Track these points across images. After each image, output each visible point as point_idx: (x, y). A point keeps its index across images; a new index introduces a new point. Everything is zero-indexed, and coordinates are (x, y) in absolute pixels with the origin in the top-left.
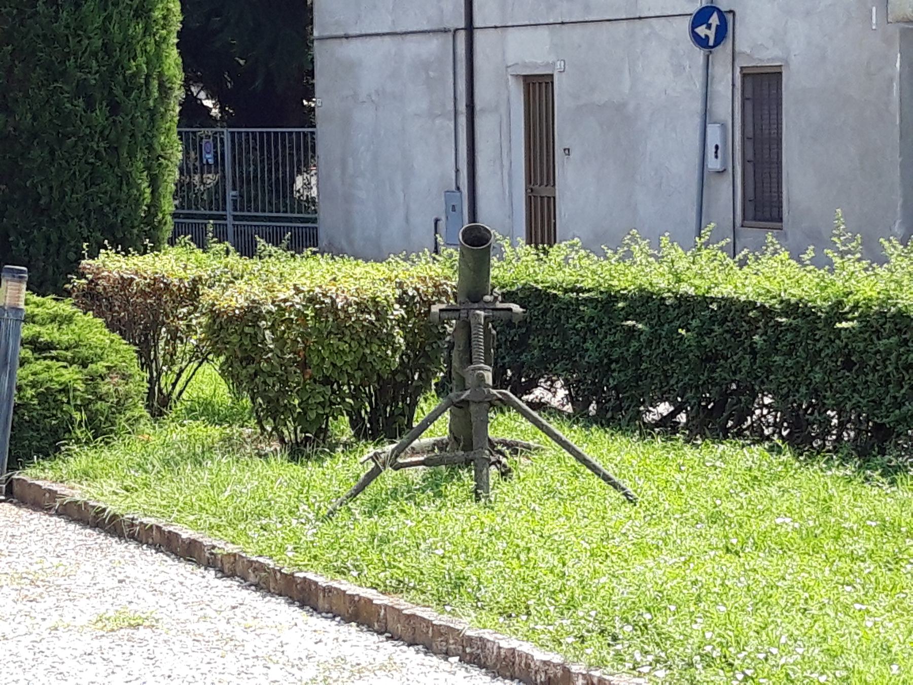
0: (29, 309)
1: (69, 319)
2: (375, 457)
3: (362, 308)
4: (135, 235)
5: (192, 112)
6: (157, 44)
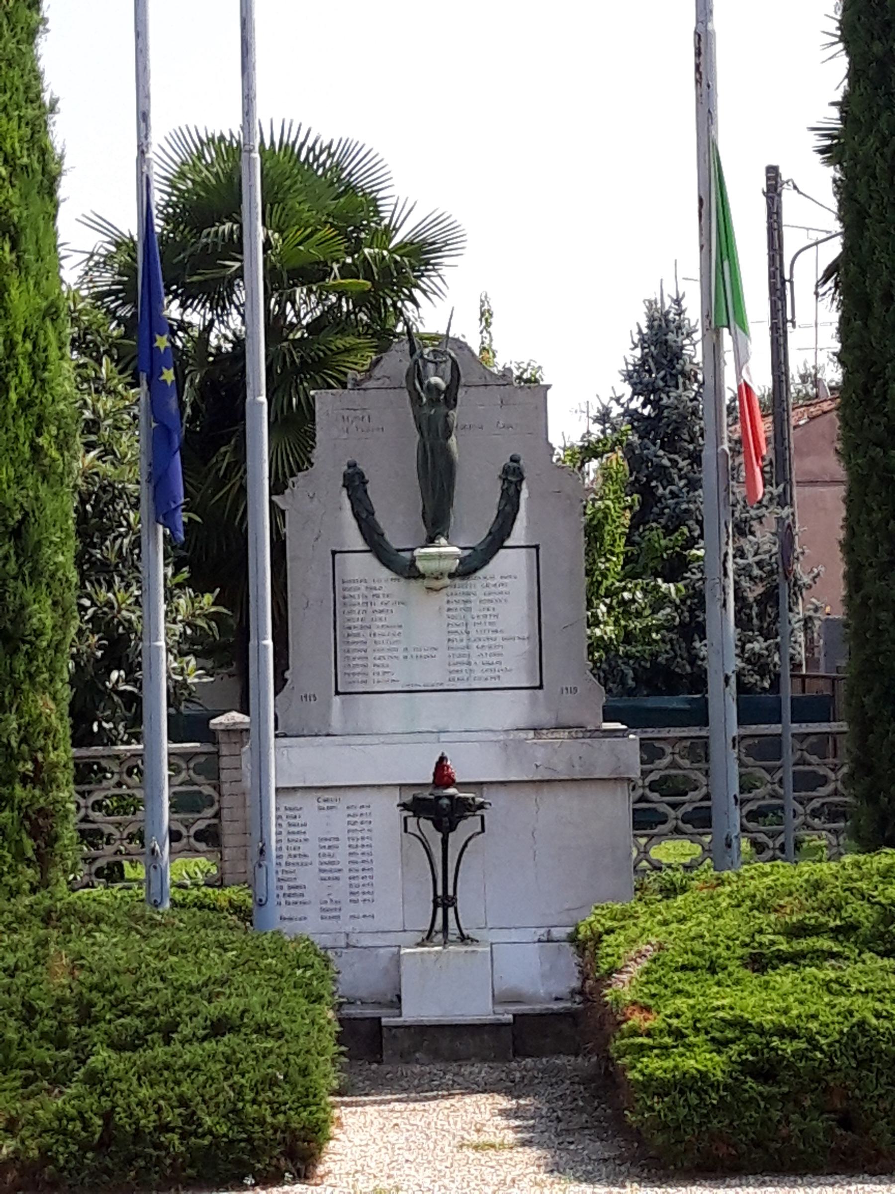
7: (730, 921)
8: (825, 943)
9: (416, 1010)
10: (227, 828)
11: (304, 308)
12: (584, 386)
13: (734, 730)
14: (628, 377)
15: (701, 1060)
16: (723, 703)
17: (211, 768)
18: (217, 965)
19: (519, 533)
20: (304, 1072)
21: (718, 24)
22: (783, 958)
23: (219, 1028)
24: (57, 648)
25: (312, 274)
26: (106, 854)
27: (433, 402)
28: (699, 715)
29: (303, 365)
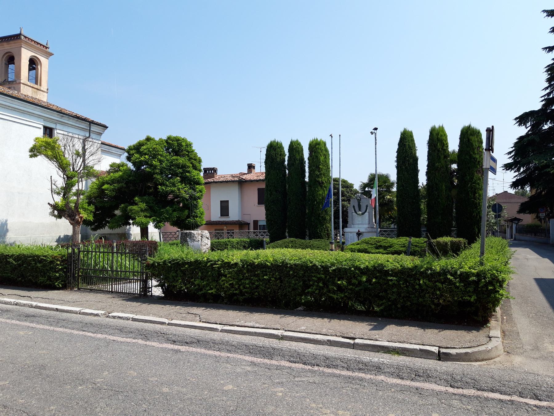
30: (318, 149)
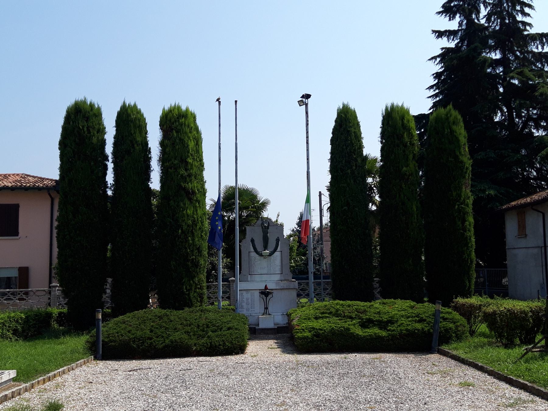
0: (442, 310)
1: (451, 313)
2: (526, 349)
3: (521, 313)
4: (466, 294)
5: (478, 265)
6: (470, 252)
7: (312, 311)
8: (327, 315)
9: (261, 326)
10: (231, 296)
11: (245, 214)
12: (289, 226)
13: (313, 281)
14: (297, 224)
15: (307, 334)
16: (311, 276)
17: (229, 287)
18: (229, 318)
19: (279, 249)
20: (243, 336)
21: (310, 170)
22: (320, 317)
23: (229, 329)
24: (204, 267)
25: (246, 208)
26: (211, 300)
27: (265, 228)
28: (307, 278)
29: (244, 222)
30: (179, 127)
